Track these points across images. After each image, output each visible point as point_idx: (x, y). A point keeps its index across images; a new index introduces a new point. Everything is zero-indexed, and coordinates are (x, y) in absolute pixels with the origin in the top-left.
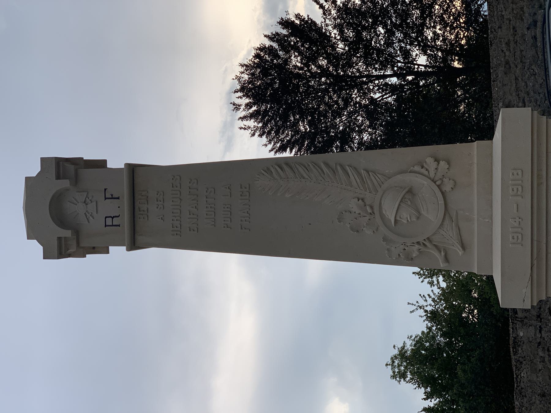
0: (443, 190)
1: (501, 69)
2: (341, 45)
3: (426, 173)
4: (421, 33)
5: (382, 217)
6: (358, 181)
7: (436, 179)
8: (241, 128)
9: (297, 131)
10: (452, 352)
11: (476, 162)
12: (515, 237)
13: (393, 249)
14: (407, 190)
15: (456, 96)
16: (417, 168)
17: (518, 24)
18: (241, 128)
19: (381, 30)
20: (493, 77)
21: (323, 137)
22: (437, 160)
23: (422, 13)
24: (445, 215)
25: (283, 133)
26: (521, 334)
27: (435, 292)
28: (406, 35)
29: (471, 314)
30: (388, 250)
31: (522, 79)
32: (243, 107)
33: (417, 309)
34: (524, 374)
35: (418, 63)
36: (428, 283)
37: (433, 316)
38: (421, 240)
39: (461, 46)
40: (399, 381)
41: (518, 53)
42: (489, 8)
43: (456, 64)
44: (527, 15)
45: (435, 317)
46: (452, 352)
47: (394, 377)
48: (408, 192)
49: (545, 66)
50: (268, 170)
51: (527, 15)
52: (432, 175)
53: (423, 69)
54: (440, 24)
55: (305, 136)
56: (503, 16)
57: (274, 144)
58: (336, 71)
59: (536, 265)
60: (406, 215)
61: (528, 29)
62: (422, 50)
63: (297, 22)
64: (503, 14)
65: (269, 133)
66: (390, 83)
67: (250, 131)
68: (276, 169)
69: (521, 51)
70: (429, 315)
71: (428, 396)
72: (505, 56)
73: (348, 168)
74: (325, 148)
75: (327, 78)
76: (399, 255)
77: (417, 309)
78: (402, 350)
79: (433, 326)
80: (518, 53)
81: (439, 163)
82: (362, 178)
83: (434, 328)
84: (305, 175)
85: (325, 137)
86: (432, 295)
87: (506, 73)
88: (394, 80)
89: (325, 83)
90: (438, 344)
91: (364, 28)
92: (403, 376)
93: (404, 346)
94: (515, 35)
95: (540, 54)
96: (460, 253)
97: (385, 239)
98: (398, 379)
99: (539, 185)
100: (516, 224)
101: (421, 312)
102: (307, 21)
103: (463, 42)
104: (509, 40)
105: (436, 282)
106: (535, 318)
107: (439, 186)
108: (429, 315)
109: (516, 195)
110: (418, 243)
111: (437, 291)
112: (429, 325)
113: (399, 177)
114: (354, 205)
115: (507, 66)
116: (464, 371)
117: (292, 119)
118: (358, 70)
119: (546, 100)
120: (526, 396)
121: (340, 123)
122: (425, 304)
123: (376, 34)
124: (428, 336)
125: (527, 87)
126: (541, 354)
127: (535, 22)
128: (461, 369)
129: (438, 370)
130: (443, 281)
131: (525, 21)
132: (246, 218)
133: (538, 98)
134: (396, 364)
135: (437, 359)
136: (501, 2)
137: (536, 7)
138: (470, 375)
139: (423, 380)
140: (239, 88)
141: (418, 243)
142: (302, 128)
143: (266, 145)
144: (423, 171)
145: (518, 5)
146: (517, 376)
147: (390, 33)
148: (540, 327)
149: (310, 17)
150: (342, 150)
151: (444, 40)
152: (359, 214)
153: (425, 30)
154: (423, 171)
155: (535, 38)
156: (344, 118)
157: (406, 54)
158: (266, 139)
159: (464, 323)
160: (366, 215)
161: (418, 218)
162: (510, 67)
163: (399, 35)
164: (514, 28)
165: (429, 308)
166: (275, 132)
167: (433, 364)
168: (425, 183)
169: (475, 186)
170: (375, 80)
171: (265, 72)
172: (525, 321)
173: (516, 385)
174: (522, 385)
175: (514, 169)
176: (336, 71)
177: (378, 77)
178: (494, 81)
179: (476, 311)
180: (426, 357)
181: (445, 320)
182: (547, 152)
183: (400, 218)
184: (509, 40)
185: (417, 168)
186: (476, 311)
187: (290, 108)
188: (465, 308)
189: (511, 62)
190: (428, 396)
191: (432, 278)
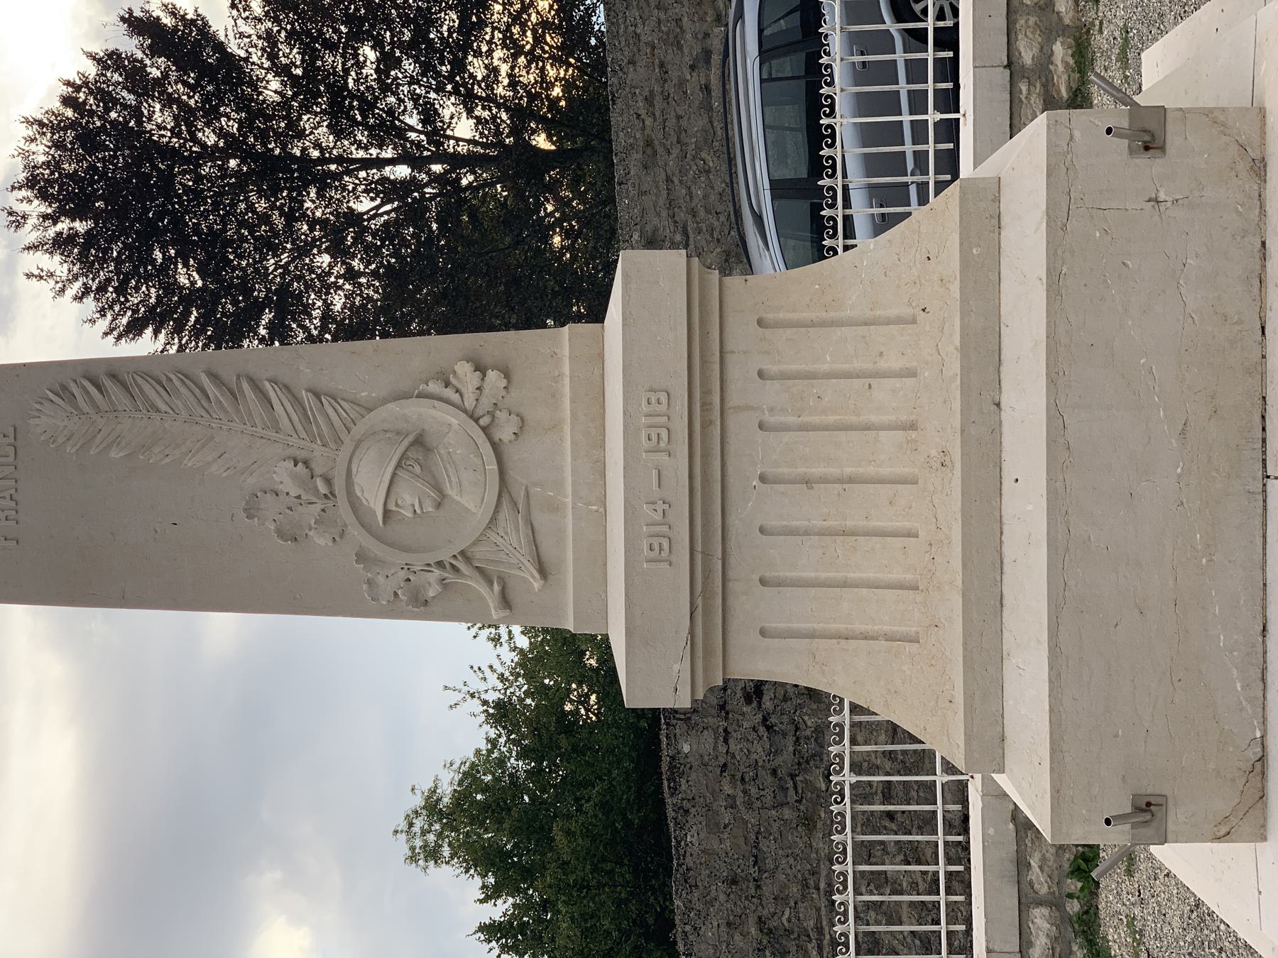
0: (496, 439)
1: (635, 156)
2: (275, 84)
3: (455, 397)
4: (459, 66)
5: (355, 505)
6: (295, 418)
7: (479, 412)
8: (29, 276)
9: (170, 287)
10: (543, 791)
11: (567, 373)
12: (656, 547)
13: (381, 579)
14: (411, 438)
15: (542, 213)
16: (434, 387)
17: (669, 57)
18: (29, 276)
19: (369, 53)
20: (619, 173)
21: (235, 303)
22: (481, 369)
23: (463, 18)
24: (500, 496)
25: (137, 289)
26: (686, 748)
27: (504, 659)
28: (427, 68)
29: (583, 705)
30: (370, 582)
31: (681, 181)
32: (33, 221)
33: (464, 700)
34: (692, 836)
35: (457, 134)
36: (490, 639)
37: (502, 713)
38: (446, 556)
39: (554, 103)
40: (425, 869)
41: (672, 122)
42: (607, 16)
43: (542, 142)
44: (689, 36)
45: (505, 716)
46: (543, 791)
47: (413, 858)
48: (412, 444)
49: (729, 153)
50: (63, 392)
51: (689, 36)
52: (469, 403)
53: (463, 149)
54: (504, 46)
55: (190, 298)
56: (637, 36)
57: (114, 319)
58: (264, 145)
59: (700, 609)
60: (409, 497)
61: (692, 67)
62: (465, 104)
63: (167, 21)
64: (638, 31)
65: (102, 289)
66: (392, 177)
67: (52, 282)
68: (84, 388)
69: (679, 117)
70: (491, 711)
71: (490, 895)
72: (644, 129)
73: (267, 385)
74: (229, 334)
75: (243, 161)
76: (396, 594)
77: (464, 700)
78: (429, 797)
79: (500, 736)
80: (672, 122)
81: (484, 375)
82: (304, 409)
83: (503, 740)
84: (163, 407)
85: (240, 302)
86: (497, 666)
87: (645, 167)
88: (403, 171)
89: (237, 173)
90: (511, 775)
91: (331, 46)
92: (433, 854)
93: (435, 791)
94: (666, 81)
95: (718, 126)
96: (536, 585)
97: (361, 557)
98: (421, 863)
99: (706, 424)
100: (658, 517)
101: (476, 706)
102: (193, 22)
103: (557, 91)
104: (651, 92)
105: (505, 637)
106: (714, 712)
107: (485, 429)
108: (491, 711)
109: (656, 450)
110: (440, 564)
111: (510, 657)
112: (492, 733)
113: (391, 406)
114: (285, 477)
115: (649, 151)
116: (569, 833)
117: (158, 255)
118: (317, 145)
119: (731, 228)
120: (696, 886)
121: (275, 270)
122: (482, 686)
123: (357, 63)
124: (490, 759)
125: (691, 198)
126: (728, 789)
127: (707, 53)
128: (562, 829)
129: (512, 834)
130: (522, 632)
131: (686, 51)
132: (6, 513)
133: (716, 223)
134: (416, 829)
135: (509, 810)
136: (635, 3)
137: (709, 19)
138: (580, 841)
139: (480, 858)
140: (22, 176)
141: (440, 564)
142: (183, 280)
143: (93, 321)
144: (449, 393)
145: (670, 13)
146: (678, 843)
147: (387, 62)
148: (725, 730)
149: (200, 11)
150: (279, 332)
151: (513, 84)
152: (299, 497)
153: (470, 58)
154: (449, 393)
155: (707, 88)
156: (285, 258)
157: (429, 114)
158: (94, 304)
159: (567, 725)
160: (314, 500)
161: (439, 505)
162: (655, 153)
163: (409, 66)
164: (662, 65)
165: (492, 697)
166: (116, 290)
167: (500, 822)
168: (454, 421)
169: (567, 429)
170: (358, 169)
171: (88, 140)
172: (695, 718)
173: (675, 862)
174: (689, 861)
175: (652, 390)
176: (264, 145)
177: (367, 164)
178: (620, 184)
179: (593, 697)
180: (485, 806)
181: (528, 722)
182: (721, 352)
183: (397, 505)
184: (651, 92)
185: (434, 387)
186: (593, 697)
187: (150, 234)
188: (569, 691)
189: (656, 142)
190: (490, 895)
191: (497, 628)
